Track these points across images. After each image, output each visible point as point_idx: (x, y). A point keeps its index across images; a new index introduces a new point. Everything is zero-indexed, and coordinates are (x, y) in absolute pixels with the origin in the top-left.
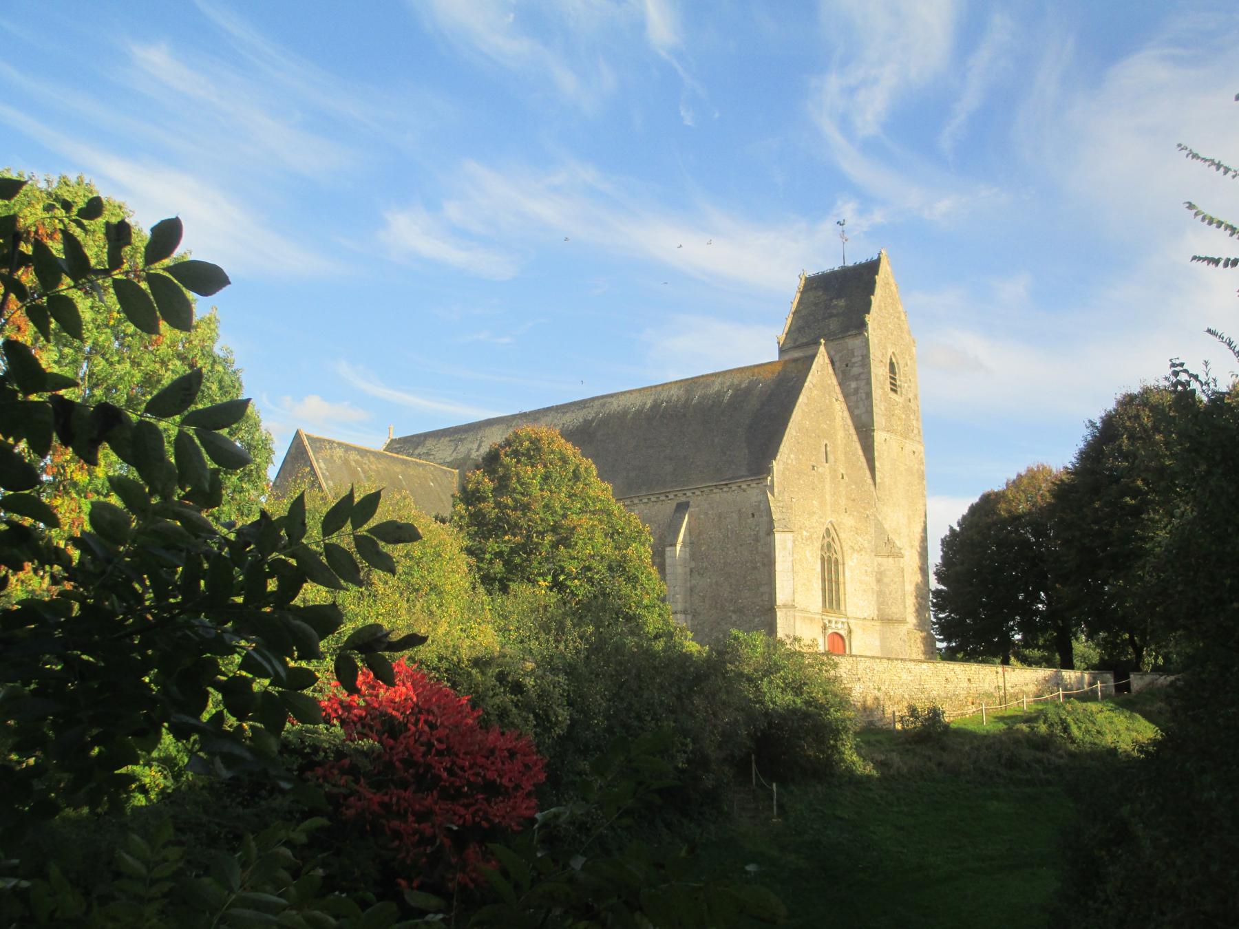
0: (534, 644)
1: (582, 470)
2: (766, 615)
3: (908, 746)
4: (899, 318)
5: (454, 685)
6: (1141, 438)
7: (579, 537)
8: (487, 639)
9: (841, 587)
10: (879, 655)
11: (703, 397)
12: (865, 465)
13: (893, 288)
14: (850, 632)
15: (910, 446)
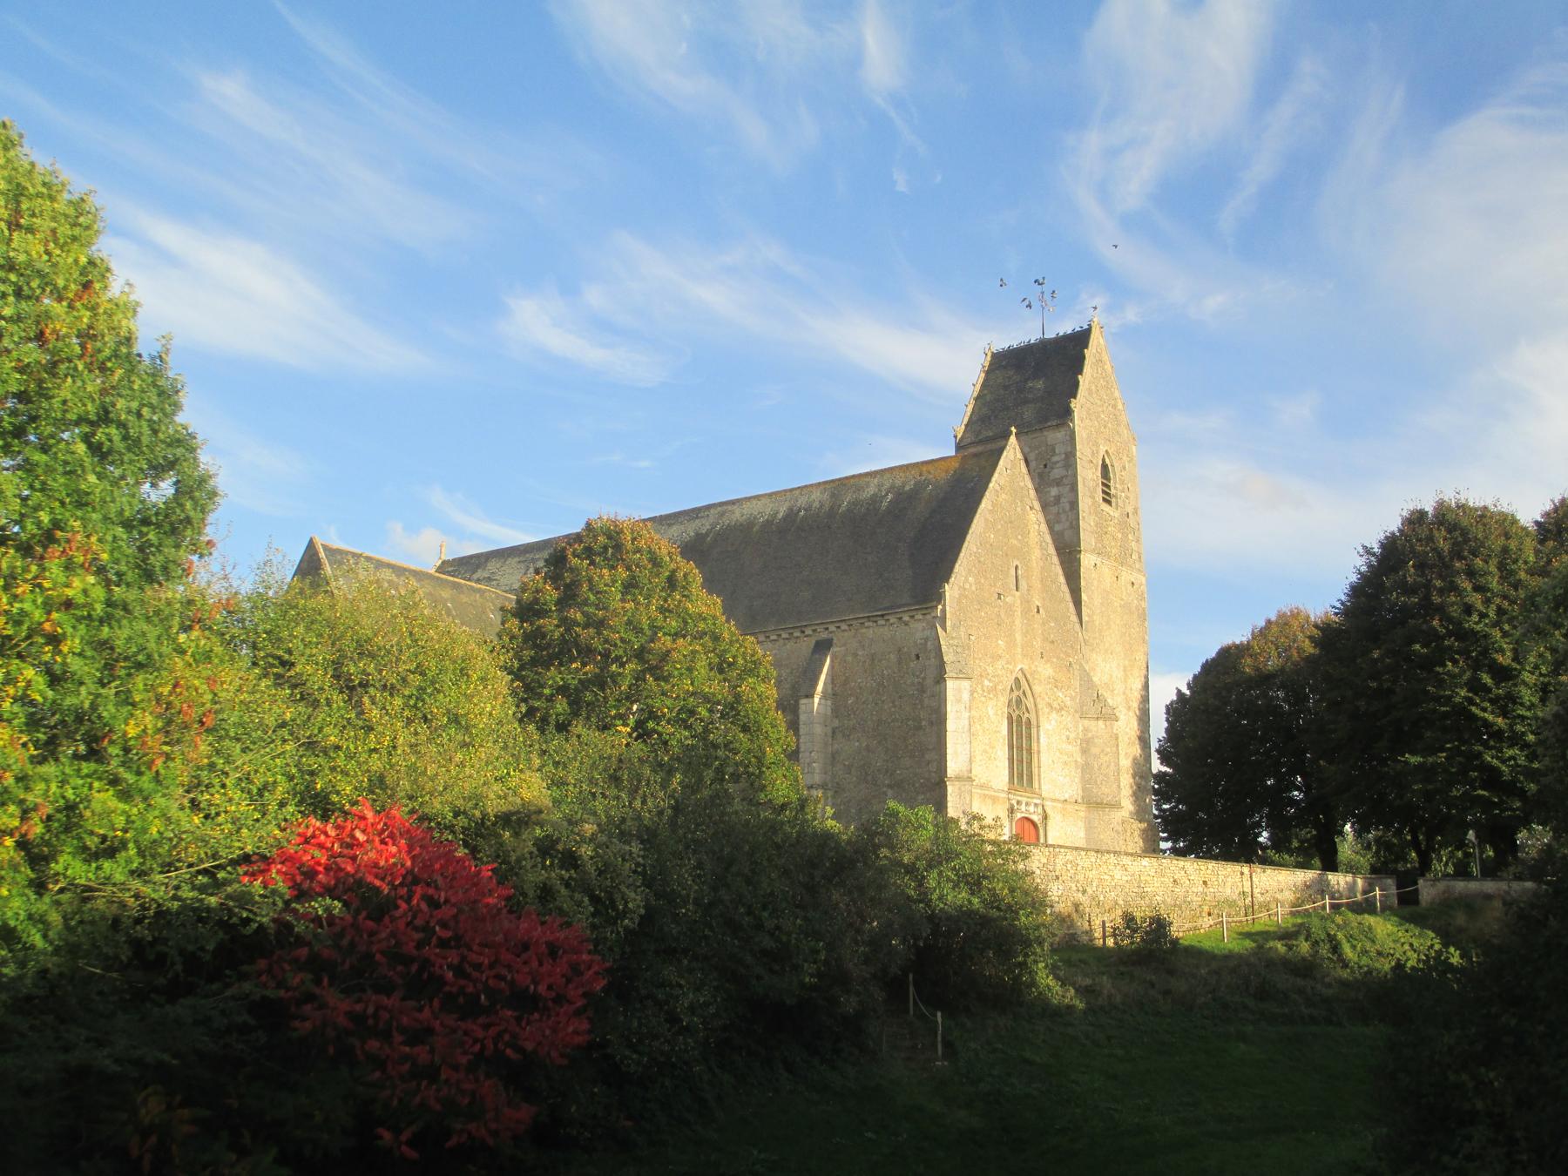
0: (599, 805)
1: (680, 575)
2: (934, 789)
3: (1122, 969)
4: (1114, 407)
5: (474, 851)
6: (1434, 566)
7: (675, 667)
8: (533, 789)
9: (1035, 757)
10: (1082, 843)
11: (855, 503)
12: (1068, 596)
13: (1108, 367)
14: (1045, 817)
15: (1127, 576)
